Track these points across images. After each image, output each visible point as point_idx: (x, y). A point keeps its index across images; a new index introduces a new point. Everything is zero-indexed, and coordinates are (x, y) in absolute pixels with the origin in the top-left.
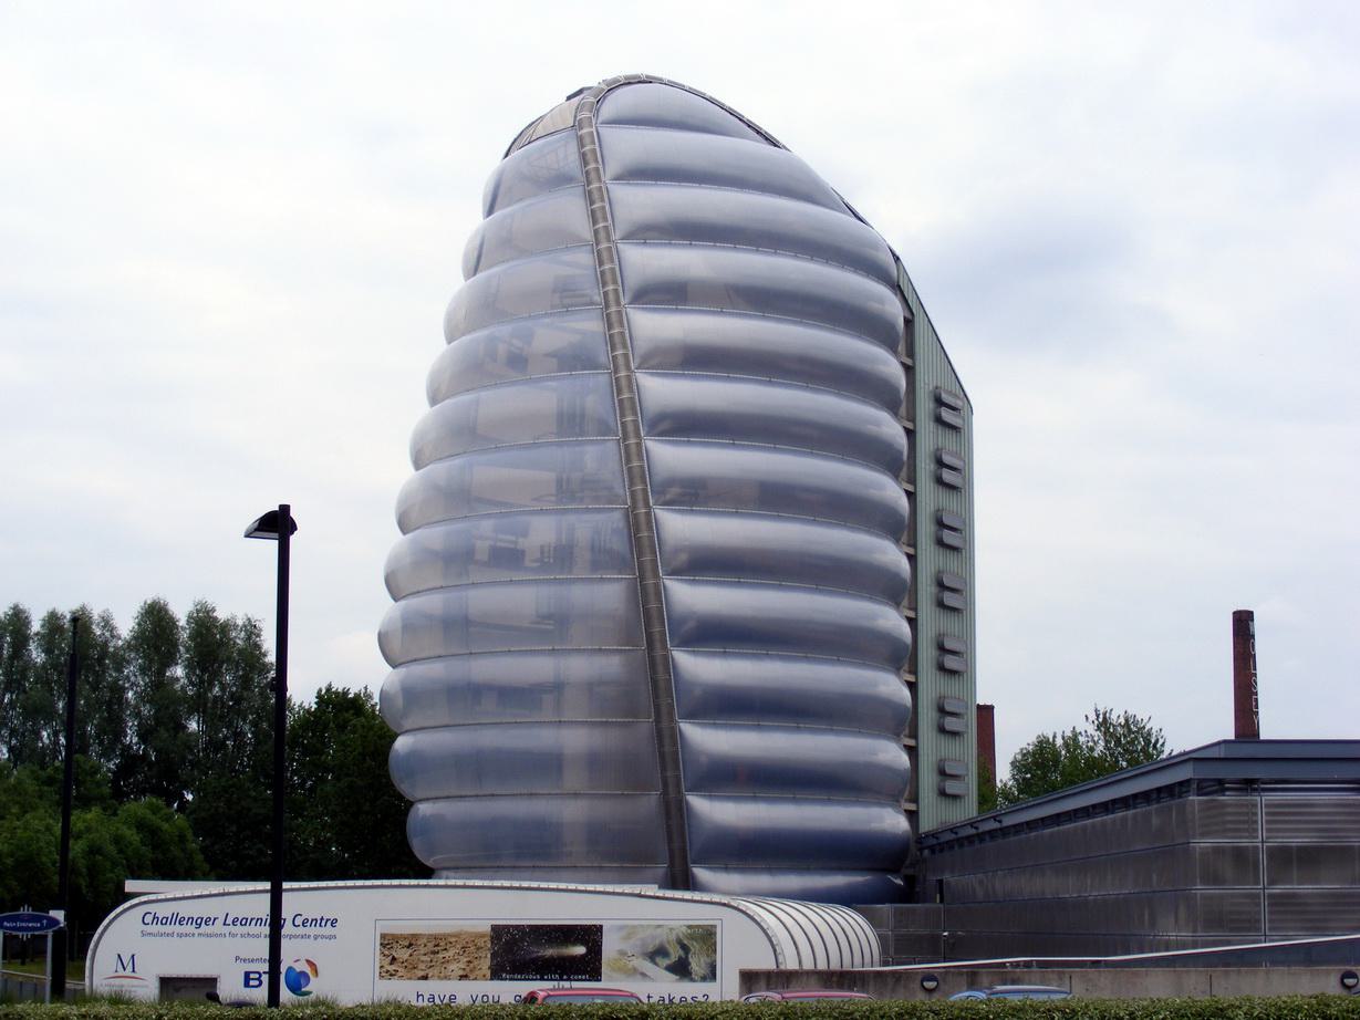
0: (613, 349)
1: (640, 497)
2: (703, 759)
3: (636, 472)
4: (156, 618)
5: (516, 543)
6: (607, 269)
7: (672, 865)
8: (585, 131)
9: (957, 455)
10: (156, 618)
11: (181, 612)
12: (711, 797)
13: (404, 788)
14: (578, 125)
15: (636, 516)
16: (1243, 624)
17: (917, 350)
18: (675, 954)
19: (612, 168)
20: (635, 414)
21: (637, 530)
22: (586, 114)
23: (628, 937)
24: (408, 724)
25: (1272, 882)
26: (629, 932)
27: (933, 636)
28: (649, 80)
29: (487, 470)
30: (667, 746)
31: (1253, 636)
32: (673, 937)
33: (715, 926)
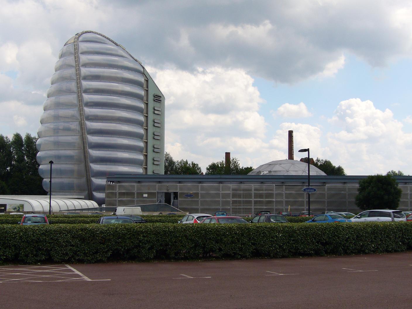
0: (78, 89)
1: (82, 119)
2: (95, 171)
3: (82, 114)
4: (18, 137)
5: (69, 126)
6: (78, 73)
7: (89, 192)
8: (75, 43)
9: (160, 108)
10: (18, 137)
11: (24, 137)
12: (96, 178)
13: (42, 176)
14: (74, 42)
15: (81, 123)
16: (291, 133)
17: (149, 86)
18: (18, 209)
19: (80, 51)
20: (82, 102)
21: (82, 126)
22: (76, 40)
23: (10, 206)
24: (42, 163)
25: (119, 198)
26: (11, 205)
27: (152, 145)
28: (90, 32)
29: (63, 112)
30: (87, 168)
31: (293, 137)
32: (17, 206)
33: (23, 204)
